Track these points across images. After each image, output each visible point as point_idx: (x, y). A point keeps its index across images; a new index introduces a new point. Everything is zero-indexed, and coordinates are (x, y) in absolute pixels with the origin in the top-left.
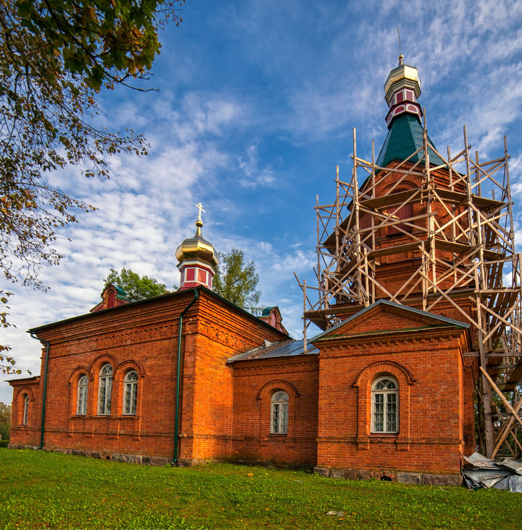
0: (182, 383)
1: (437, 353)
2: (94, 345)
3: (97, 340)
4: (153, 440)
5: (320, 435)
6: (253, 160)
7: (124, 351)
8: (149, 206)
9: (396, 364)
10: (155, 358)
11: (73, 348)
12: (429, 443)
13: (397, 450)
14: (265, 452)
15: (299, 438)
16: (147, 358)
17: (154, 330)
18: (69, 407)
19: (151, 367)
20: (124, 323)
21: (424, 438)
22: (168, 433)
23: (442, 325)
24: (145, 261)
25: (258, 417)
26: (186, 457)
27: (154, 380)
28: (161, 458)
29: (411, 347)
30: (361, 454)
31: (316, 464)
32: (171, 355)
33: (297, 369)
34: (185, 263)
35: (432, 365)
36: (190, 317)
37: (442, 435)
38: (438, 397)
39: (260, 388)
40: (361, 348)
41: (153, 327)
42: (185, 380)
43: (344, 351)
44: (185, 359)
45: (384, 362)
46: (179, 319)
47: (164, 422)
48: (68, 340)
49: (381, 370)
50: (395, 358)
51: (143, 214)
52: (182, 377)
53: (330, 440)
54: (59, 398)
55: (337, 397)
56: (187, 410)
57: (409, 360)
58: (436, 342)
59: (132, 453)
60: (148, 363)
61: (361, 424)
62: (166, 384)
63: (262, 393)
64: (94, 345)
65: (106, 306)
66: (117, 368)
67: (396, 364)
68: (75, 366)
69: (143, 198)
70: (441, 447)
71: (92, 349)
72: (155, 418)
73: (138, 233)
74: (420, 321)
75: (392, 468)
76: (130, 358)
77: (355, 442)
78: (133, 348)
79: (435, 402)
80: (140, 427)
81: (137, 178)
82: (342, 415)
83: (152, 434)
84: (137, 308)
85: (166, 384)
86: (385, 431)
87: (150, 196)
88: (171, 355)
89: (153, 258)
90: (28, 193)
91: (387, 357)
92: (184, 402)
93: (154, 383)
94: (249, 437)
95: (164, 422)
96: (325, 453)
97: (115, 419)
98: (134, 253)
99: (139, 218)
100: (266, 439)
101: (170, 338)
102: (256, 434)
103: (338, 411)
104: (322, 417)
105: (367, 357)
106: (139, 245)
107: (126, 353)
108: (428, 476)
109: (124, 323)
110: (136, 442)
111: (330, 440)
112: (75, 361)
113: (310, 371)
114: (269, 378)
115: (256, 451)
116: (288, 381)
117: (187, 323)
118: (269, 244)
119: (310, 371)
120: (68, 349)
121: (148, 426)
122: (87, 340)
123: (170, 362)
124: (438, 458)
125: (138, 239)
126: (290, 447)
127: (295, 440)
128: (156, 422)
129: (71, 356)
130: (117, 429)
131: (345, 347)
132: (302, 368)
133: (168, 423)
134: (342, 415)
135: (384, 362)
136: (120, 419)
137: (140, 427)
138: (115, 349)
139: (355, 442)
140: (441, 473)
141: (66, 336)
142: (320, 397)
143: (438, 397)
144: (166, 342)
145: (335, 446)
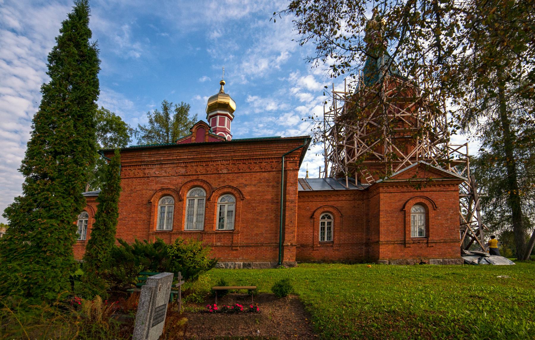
0: (285, 206)
1: (448, 193)
2: (182, 171)
3: (186, 166)
4: (253, 249)
5: (381, 240)
6: (127, 36)
7: (220, 178)
8: (30, 49)
9: (427, 198)
10: (255, 185)
11: (154, 171)
12: (445, 242)
13: (428, 246)
14: (316, 254)
15: (342, 244)
16: (246, 185)
17: (253, 163)
18: (149, 223)
19: (251, 193)
20: (222, 155)
21: (442, 239)
22: (269, 243)
23: (452, 178)
24: (23, 97)
25: (311, 231)
26: (289, 260)
27: (254, 203)
28: (264, 263)
29: (434, 189)
30: (406, 250)
31: (378, 258)
32: (271, 184)
33: (340, 199)
34: (210, 115)
35: (445, 200)
36: (292, 157)
37: (451, 238)
38: (449, 217)
39: (313, 210)
40: (406, 187)
41: (252, 161)
42: (287, 203)
43: (395, 189)
44: (288, 188)
45: (421, 197)
46: (282, 158)
47: (265, 235)
48: (152, 163)
49: (418, 202)
50: (426, 194)
51: (24, 56)
52: (285, 201)
53: (388, 243)
54: (134, 215)
55: (392, 217)
56: (290, 225)
57: (434, 196)
58: (447, 187)
59: (230, 260)
60: (248, 189)
61: (407, 232)
62: (267, 206)
63: (315, 214)
64: (182, 171)
65: (194, 138)
66: (214, 191)
67: (427, 198)
68: (158, 186)
69: (24, 40)
70: (452, 244)
71: (179, 174)
72: (256, 232)
73: (18, 71)
74: (440, 175)
75: (425, 257)
76: (226, 184)
77: (404, 243)
78: (230, 176)
79: (447, 219)
80: (238, 239)
81: (20, 21)
82: (394, 227)
83: (253, 245)
84: (240, 145)
85: (267, 206)
86: (326, 240)
87: (32, 39)
88: (271, 184)
89: (28, 95)
90: (479, 62)
91: (421, 194)
92: (287, 220)
93: (254, 205)
94: (304, 245)
95: (265, 235)
96: (384, 251)
97: (211, 234)
98: (11, 88)
99: (19, 58)
100: (319, 245)
101: (269, 172)
102: (310, 242)
103: (392, 225)
104: (382, 229)
105: (409, 193)
106: (17, 83)
107: (221, 180)
108: (447, 260)
109: (222, 155)
110: (235, 252)
111: (388, 243)
112: (156, 183)
113: (350, 201)
114: (320, 204)
115: (310, 254)
116: (335, 206)
117: (288, 162)
118: (132, 102)
119: (350, 201)
120: (147, 171)
121: (247, 239)
122: (171, 166)
123: (270, 189)
124: (450, 250)
125: (15, 76)
126: (335, 250)
127: (340, 245)
128: (257, 235)
129: (151, 178)
130: (213, 242)
131: (397, 186)
132: (344, 198)
133: (269, 235)
134: (394, 227)
135: (421, 197)
136: (216, 233)
137: (238, 239)
138: (209, 176)
139: (404, 243)
140: (452, 258)
141: (146, 160)
142: (381, 216)
143: (449, 217)
144: (265, 174)
145: (391, 247)
